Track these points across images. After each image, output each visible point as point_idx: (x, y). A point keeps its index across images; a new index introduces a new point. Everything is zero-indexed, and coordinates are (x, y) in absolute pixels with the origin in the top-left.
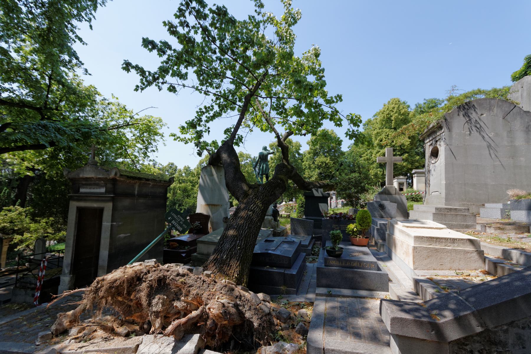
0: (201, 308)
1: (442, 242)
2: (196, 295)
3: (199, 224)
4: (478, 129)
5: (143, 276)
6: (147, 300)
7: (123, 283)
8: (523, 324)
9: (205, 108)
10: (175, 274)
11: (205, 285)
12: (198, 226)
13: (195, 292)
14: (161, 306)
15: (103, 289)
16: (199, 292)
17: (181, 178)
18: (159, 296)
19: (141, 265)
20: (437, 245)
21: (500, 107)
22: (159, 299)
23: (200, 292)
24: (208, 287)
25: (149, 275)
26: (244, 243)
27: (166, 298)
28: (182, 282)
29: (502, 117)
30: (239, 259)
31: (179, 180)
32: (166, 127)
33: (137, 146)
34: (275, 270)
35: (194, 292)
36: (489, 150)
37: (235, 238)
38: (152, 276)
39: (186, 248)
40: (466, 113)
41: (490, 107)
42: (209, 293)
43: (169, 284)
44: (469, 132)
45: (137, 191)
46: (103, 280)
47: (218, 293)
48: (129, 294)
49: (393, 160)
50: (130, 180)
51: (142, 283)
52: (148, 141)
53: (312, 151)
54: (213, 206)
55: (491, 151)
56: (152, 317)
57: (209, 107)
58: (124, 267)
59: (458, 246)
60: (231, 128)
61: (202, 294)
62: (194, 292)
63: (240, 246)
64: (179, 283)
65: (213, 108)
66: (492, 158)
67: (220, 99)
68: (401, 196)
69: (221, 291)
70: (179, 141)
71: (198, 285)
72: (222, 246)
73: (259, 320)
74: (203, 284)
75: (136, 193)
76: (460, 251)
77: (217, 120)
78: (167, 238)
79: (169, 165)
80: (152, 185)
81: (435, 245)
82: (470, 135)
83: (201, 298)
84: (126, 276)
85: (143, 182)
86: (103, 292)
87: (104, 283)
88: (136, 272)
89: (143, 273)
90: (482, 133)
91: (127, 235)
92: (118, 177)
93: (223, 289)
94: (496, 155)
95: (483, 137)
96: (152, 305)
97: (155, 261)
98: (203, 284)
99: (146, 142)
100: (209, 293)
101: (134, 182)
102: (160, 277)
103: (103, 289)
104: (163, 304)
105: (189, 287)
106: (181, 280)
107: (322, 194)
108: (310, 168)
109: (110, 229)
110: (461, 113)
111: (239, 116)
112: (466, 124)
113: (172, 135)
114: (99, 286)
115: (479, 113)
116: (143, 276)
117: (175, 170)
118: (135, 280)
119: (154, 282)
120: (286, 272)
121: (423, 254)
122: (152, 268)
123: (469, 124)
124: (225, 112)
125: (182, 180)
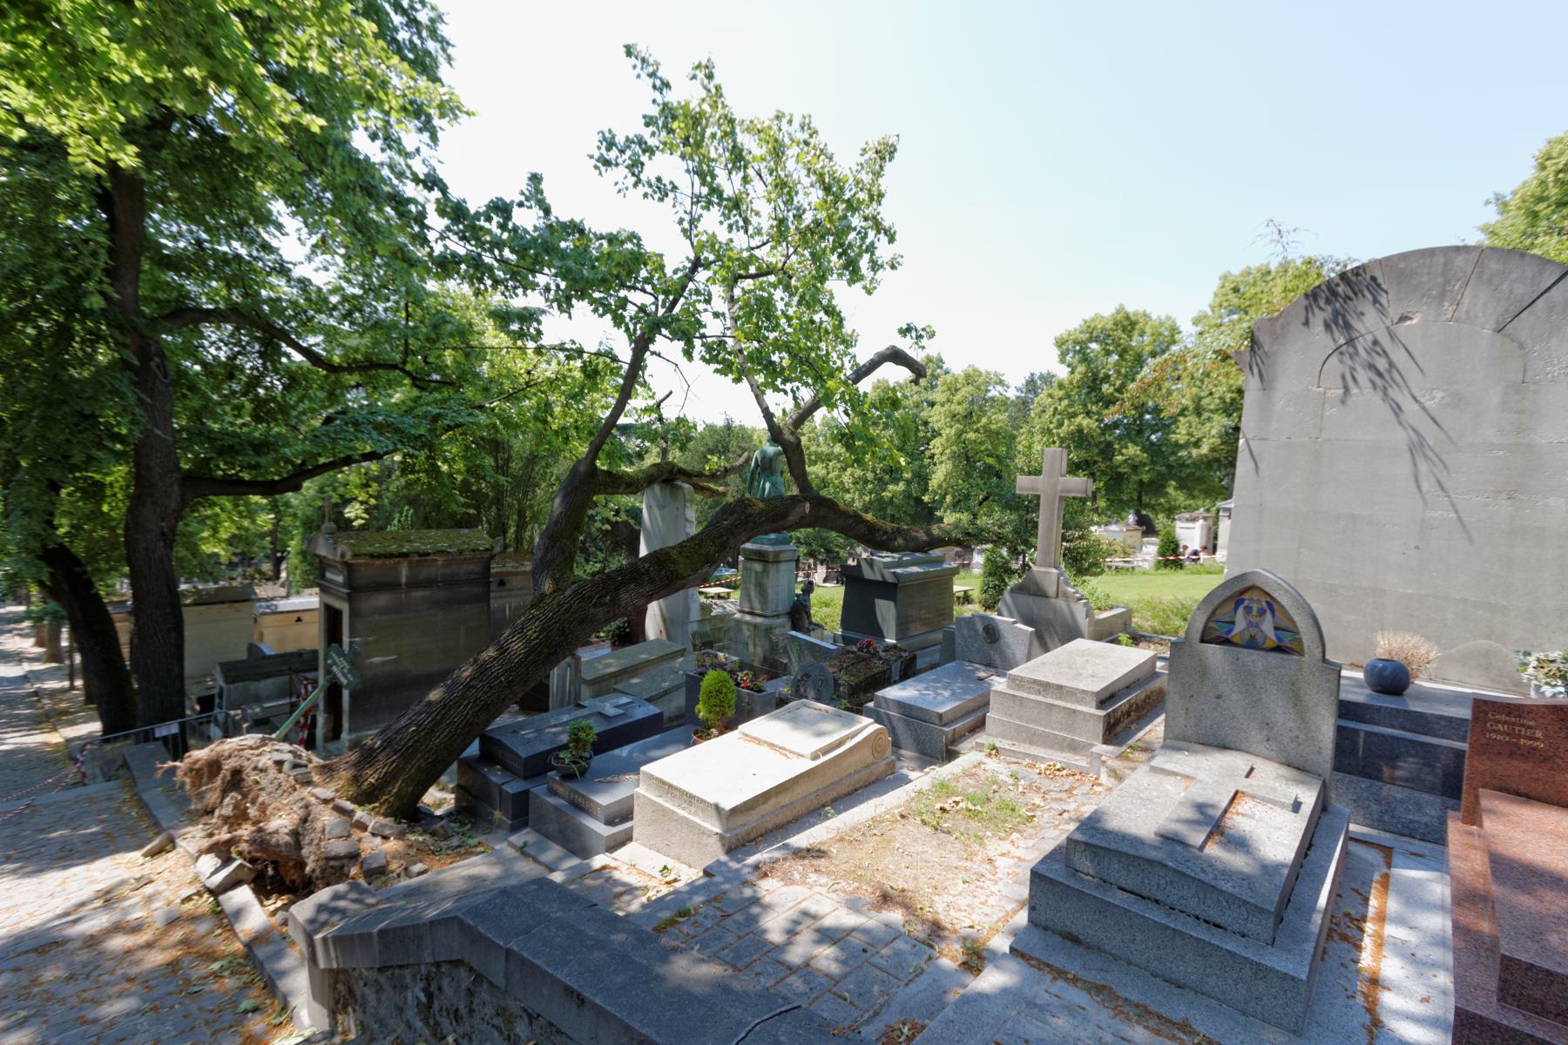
4: (1380, 375)
21: (1490, 280)
29: (1491, 324)
36: (1415, 464)
40: (1336, 313)
41: (1447, 282)
44: (1341, 391)
49: (1059, 488)
55: (1423, 467)
59: (695, 814)
66: (1419, 487)
68: (1072, 604)
75: (404, 580)
76: (696, 825)
82: (1343, 402)
90: (1394, 393)
94: (1438, 482)
95: (1397, 409)
107: (882, 575)
108: (1198, 411)
110: (1318, 319)
112: (1334, 360)
115: (1394, 313)
123: (1346, 359)
125: (816, 453)
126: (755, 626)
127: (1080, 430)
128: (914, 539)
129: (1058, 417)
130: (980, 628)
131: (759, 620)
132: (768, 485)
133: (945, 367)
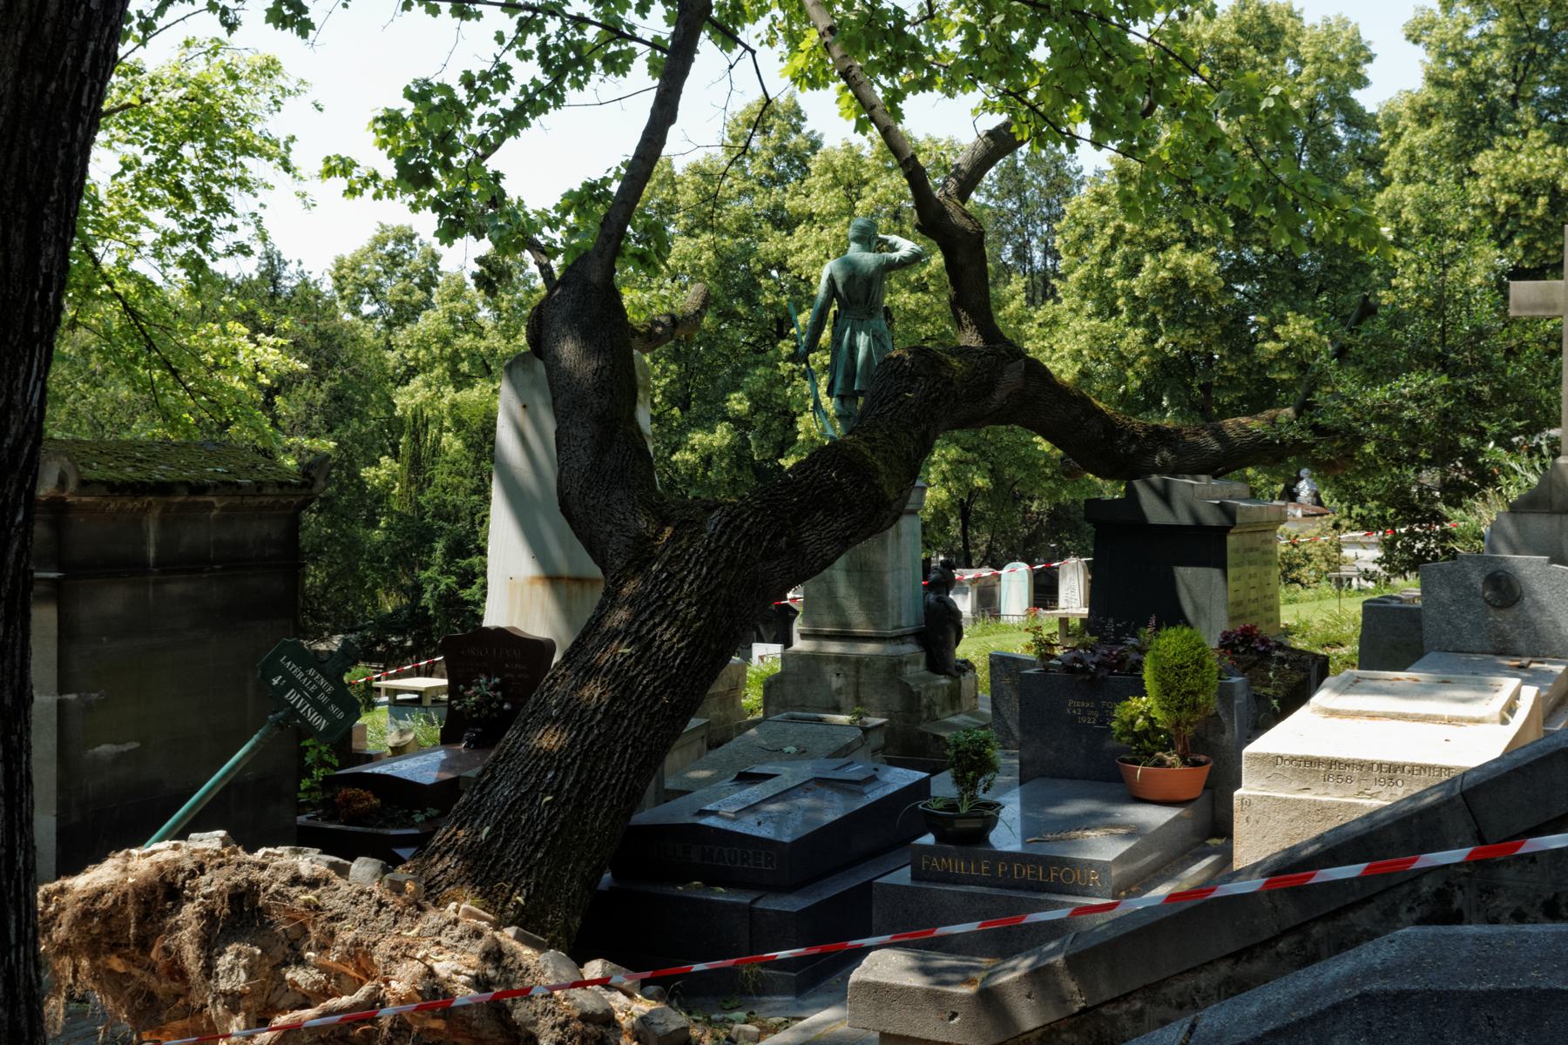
0: (367, 988)
1: (1349, 779)
2: (351, 944)
3: (495, 688)
5: (184, 883)
6: (199, 958)
7: (125, 902)
8: (1180, 995)
9: (468, 80)
10: (285, 877)
11: (383, 916)
12: (492, 700)
13: (349, 937)
14: (243, 976)
15: (66, 917)
16: (364, 937)
17: (465, 341)
18: (236, 946)
19: (176, 848)
20: (1330, 790)
22: (238, 956)
23: (368, 938)
24: (396, 922)
25: (204, 879)
26: (576, 781)
27: (261, 955)
28: (307, 904)
30: (542, 840)
31: (455, 358)
32: (304, 101)
33: (150, 225)
34: (720, 895)
35: (347, 934)
37: (540, 759)
38: (212, 883)
39: (419, 818)
42: (397, 940)
43: (267, 910)
45: (158, 546)
46: (62, 891)
47: (427, 942)
48: (144, 944)
50: (120, 501)
51: (182, 905)
52: (205, 192)
53: (1451, 95)
54: (575, 588)
56: (219, 1008)
57: (485, 76)
58: (123, 853)
60: (606, 181)
61: (375, 944)
62: (347, 934)
63: (556, 793)
64: (298, 905)
65: (509, 77)
67: (540, 27)
69: (438, 939)
70: (377, 196)
71: (362, 915)
72: (487, 790)
73: (557, 1030)
74: (377, 913)
75: (152, 553)
77: (538, 126)
78: (323, 764)
79: (380, 242)
80: (223, 509)
81: (1322, 791)
83: (368, 955)
84: (130, 880)
85: (179, 499)
86: (64, 927)
87: (68, 898)
88: (161, 869)
89: (183, 870)
91: (125, 748)
92: (72, 494)
93: (444, 932)
96: (217, 974)
97: (222, 839)
98: (377, 913)
99: (197, 198)
100: (397, 940)
101: (138, 504)
102: (237, 886)
103: (66, 917)
104: (251, 974)
105: (332, 919)
106: (304, 897)
109: (54, 719)
111: (653, 93)
113: (329, 172)
114: (51, 909)
116: (184, 883)
117: (428, 283)
118: (160, 893)
119: (219, 901)
120: (760, 905)
121: (1273, 829)
122: (211, 857)
124: (580, 86)
125: (472, 354)
126: (859, 662)
127: (1179, 280)
128: (1196, 448)
129: (1123, 249)
130: (1477, 579)
131: (869, 649)
132: (862, 340)
133: (807, 128)
